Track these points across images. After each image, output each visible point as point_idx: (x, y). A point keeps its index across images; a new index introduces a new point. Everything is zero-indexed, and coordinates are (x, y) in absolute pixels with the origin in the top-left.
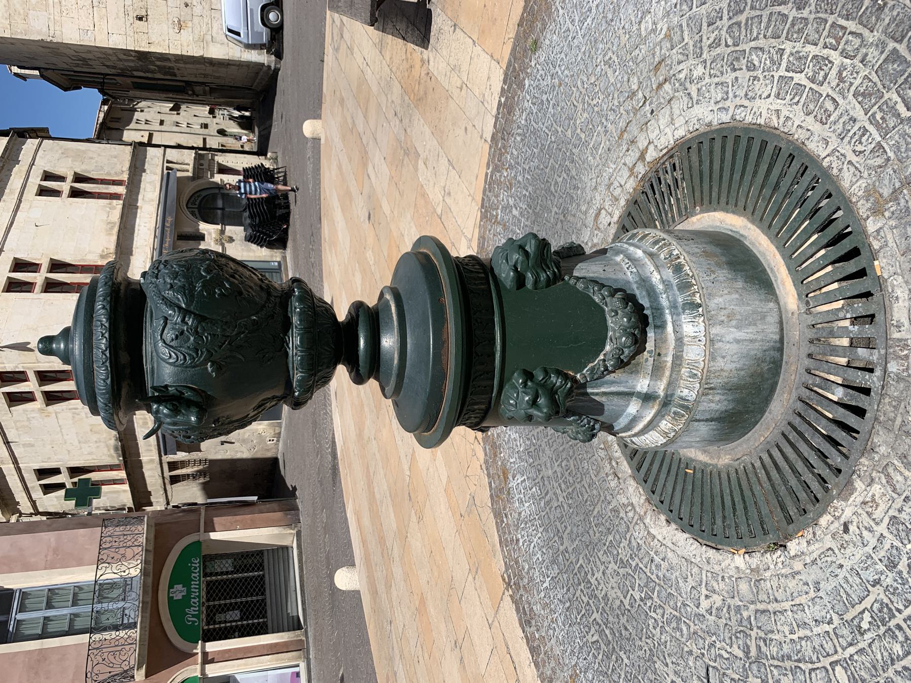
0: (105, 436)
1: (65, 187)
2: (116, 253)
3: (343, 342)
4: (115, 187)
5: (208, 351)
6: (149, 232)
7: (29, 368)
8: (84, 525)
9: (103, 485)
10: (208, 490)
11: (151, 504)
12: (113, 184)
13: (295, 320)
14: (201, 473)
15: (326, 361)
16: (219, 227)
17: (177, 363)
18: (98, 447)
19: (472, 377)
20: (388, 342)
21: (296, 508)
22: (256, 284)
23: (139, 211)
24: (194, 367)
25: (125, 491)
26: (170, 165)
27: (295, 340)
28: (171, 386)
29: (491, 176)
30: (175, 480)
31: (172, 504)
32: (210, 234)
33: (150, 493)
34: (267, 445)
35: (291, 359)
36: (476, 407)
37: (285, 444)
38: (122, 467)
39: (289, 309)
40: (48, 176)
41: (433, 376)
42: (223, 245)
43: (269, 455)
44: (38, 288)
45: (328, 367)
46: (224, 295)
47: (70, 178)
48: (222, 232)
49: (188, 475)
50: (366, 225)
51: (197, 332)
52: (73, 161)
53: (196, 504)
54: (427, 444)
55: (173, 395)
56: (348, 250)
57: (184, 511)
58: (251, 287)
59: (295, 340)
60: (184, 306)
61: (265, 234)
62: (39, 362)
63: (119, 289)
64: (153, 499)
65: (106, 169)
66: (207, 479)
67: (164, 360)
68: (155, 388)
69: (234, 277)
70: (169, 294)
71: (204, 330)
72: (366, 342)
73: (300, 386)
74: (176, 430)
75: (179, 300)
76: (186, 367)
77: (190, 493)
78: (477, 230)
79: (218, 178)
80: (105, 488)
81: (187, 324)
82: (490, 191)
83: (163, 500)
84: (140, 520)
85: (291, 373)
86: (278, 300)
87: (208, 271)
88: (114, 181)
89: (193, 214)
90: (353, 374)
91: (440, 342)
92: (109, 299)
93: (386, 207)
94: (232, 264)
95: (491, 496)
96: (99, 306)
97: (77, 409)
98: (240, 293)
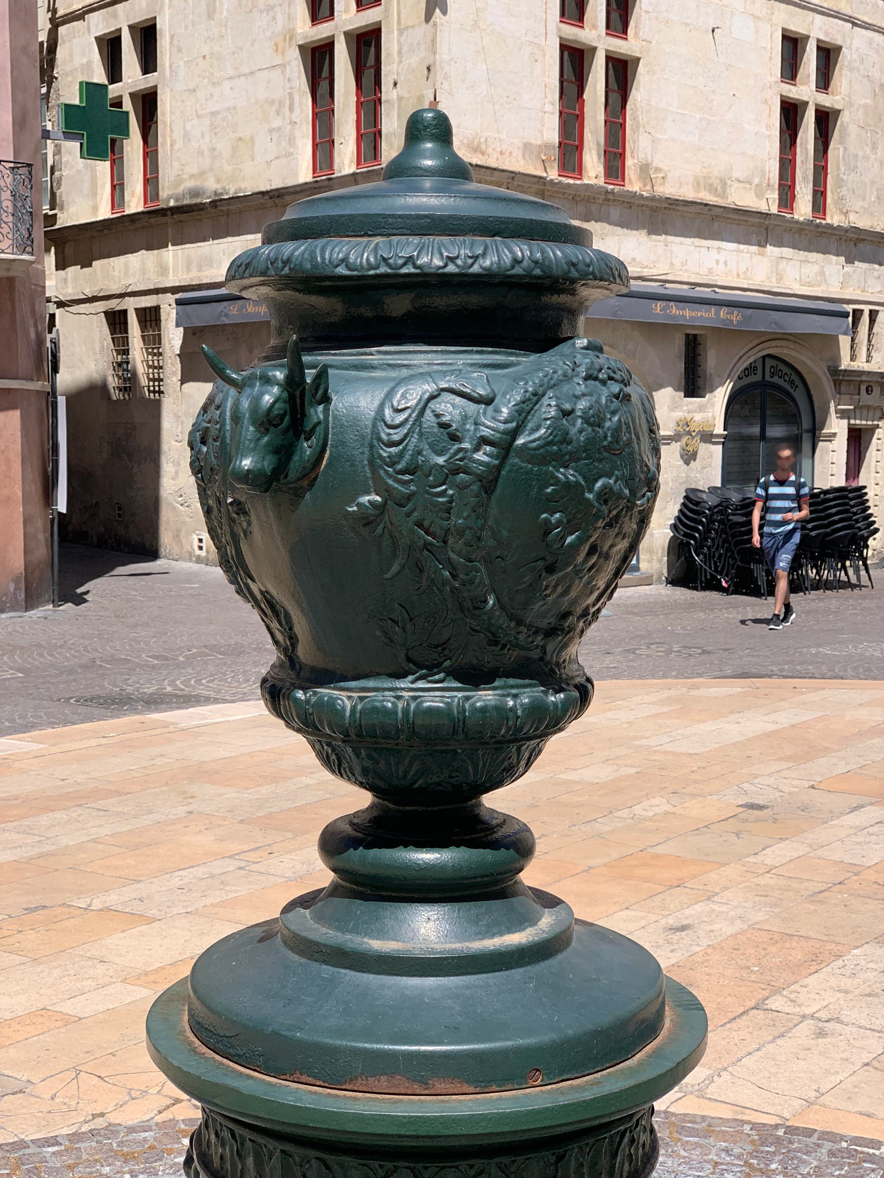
0: (228, 168)
1: (805, 90)
2: (653, 199)
3: (427, 810)
4: (809, 197)
5: (409, 497)
6: (704, 270)
7: (387, 10)
8: (20, 123)
9: (113, 163)
10: (89, 396)
11: (61, 265)
12: (815, 192)
13: (485, 697)
14: (129, 382)
15: (382, 766)
16: (719, 430)
17: (381, 426)
18: (201, 153)
19: (331, 1159)
20: (428, 928)
21: (31, 602)
22: (575, 602)
23: (754, 249)
24: (371, 463)
25: (95, 209)
26: (866, 318)
27: (436, 696)
28: (326, 411)
29: (871, 1158)
30: (117, 321)
31: (58, 312)
32: (702, 409)
33: (86, 263)
34: (188, 534)
35: (388, 683)
36: (250, 1161)
37: (190, 577)
38: (152, 206)
39: (511, 681)
40: (828, 56)
41: (335, 1051)
42: (676, 438)
43: (166, 539)
44: (571, 32)
45: (365, 771)
46: (547, 533)
47: (826, 101)
48: (708, 437)
49: (126, 352)
50: (733, 799)
51: (456, 471)
52: (866, 106)
53: (55, 369)
54: (158, 1018)
55: (304, 415)
56: (668, 748)
57: (41, 341)
58: (566, 592)
59: (436, 696)
60: (520, 441)
61: (705, 537)
62: (401, 32)
63: (560, 292)
64: (73, 271)
65: (850, 178)
66: (115, 395)
67: (389, 395)
68: (322, 375)
69: (590, 553)
70: (548, 408)
71: (462, 488)
72: (429, 867)
73: (320, 704)
74: (222, 415)
75: (538, 428)
76: (371, 446)
77: (83, 355)
78: (726, 1113)
79: (837, 427)
80: (104, 167)
81: (477, 449)
82: (831, 1153)
83: (69, 292)
84: (26, 243)
85: (353, 684)
86: (535, 654)
87: (605, 496)
88: (824, 194)
89: (750, 370)
90: (348, 829)
91: (424, 1072)
92: (537, 272)
93: (779, 853)
94: (622, 545)
95: (22, 1145)
96: (521, 250)
97: (291, 109)
98: (551, 569)
